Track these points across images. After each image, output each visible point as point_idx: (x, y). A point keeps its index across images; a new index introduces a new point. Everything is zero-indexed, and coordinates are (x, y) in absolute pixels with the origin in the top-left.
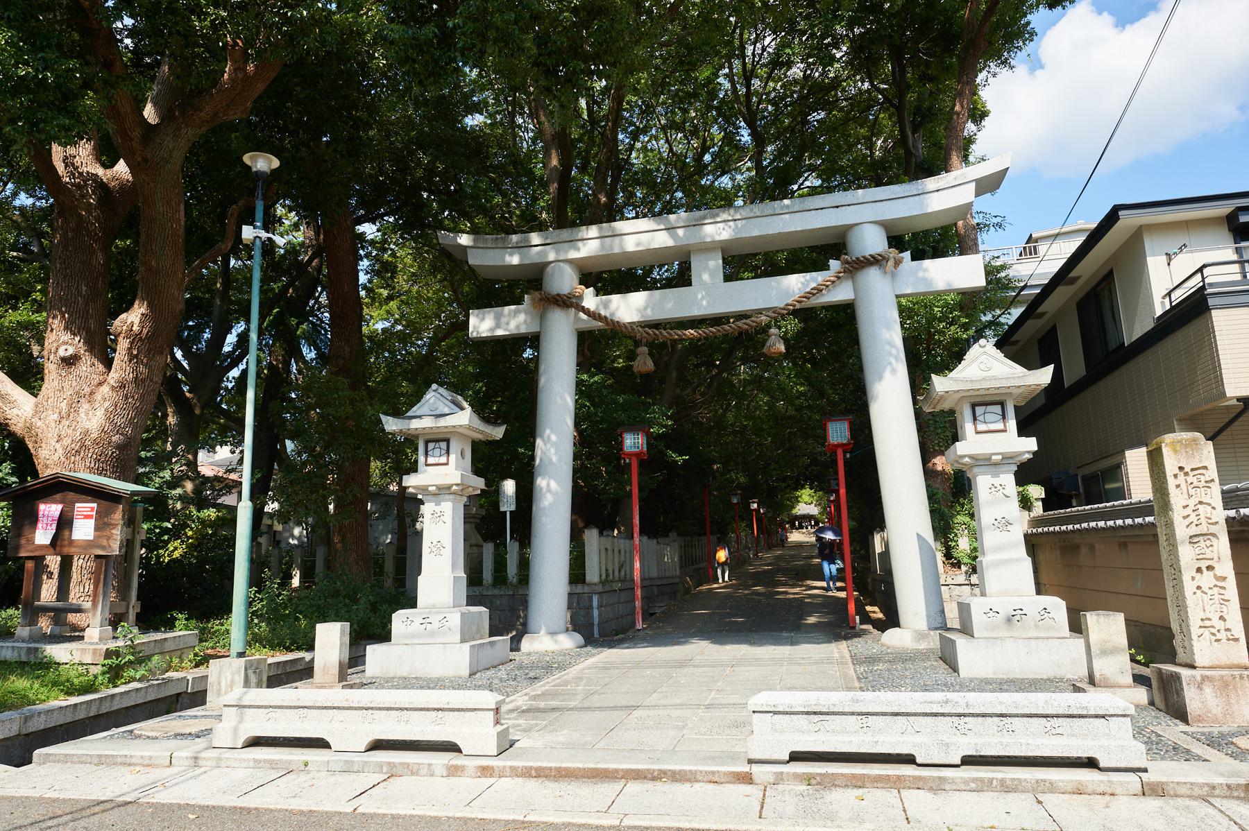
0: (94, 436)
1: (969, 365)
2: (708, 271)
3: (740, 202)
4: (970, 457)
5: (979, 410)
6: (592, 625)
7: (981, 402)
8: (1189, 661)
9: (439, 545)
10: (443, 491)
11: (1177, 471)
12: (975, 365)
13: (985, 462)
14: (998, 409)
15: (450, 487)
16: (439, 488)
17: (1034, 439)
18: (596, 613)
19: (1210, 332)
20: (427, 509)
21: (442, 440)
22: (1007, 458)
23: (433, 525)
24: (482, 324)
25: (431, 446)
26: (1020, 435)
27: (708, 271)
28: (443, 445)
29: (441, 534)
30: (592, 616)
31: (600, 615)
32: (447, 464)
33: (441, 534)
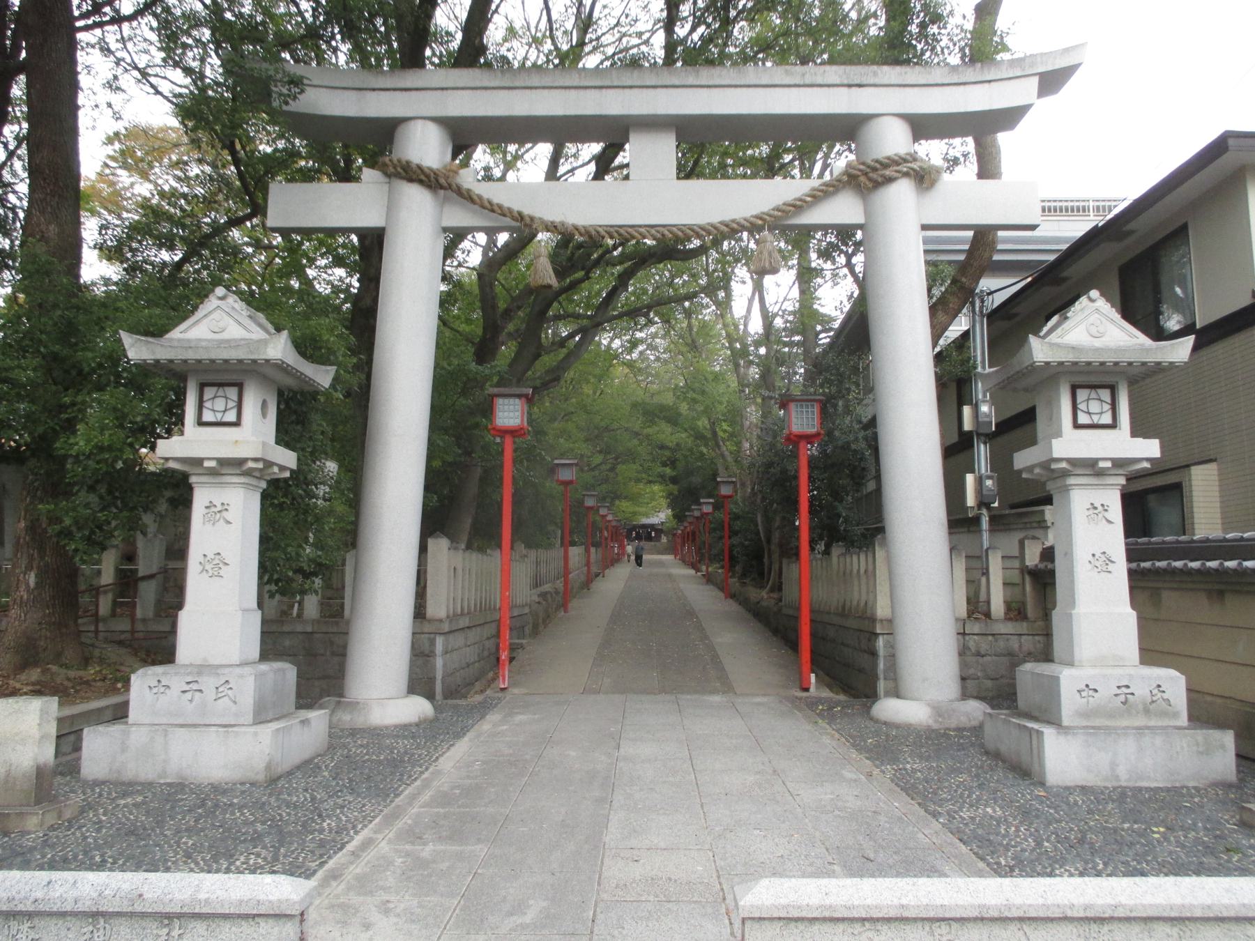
0: (123, 894)
1: (1075, 326)
2: (651, 157)
3: (679, 64)
4: (1069, 461)
5: (1082, 395)
6: (432, 680)
7: (1092, 377)
8: (1244, 762)
9: (217, 564)
10: (230, 466)
11: (1091, 558)
12: (1082, 327)
13: (1090, 467)
14: (1105, 394)
15: (240, 462)
16: (223, 462)
17: (1157, 441)
18: (439, 662)
19: (1035, 430)
20: (202, 498)
21: (227, 376)
22: (1118, 463)
23: (209, 526)
24: (297, 204)
25: (209, 392)
26: (1134, 434)
27: (651, 157)
28: (232, 393)
29: (224, 540)
30: (434, 668)
31: (445, 665)
32: (237, 424)
33: (224, 540)
